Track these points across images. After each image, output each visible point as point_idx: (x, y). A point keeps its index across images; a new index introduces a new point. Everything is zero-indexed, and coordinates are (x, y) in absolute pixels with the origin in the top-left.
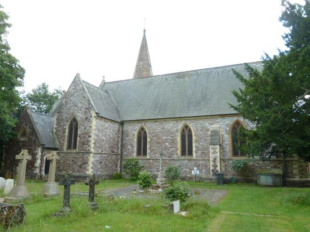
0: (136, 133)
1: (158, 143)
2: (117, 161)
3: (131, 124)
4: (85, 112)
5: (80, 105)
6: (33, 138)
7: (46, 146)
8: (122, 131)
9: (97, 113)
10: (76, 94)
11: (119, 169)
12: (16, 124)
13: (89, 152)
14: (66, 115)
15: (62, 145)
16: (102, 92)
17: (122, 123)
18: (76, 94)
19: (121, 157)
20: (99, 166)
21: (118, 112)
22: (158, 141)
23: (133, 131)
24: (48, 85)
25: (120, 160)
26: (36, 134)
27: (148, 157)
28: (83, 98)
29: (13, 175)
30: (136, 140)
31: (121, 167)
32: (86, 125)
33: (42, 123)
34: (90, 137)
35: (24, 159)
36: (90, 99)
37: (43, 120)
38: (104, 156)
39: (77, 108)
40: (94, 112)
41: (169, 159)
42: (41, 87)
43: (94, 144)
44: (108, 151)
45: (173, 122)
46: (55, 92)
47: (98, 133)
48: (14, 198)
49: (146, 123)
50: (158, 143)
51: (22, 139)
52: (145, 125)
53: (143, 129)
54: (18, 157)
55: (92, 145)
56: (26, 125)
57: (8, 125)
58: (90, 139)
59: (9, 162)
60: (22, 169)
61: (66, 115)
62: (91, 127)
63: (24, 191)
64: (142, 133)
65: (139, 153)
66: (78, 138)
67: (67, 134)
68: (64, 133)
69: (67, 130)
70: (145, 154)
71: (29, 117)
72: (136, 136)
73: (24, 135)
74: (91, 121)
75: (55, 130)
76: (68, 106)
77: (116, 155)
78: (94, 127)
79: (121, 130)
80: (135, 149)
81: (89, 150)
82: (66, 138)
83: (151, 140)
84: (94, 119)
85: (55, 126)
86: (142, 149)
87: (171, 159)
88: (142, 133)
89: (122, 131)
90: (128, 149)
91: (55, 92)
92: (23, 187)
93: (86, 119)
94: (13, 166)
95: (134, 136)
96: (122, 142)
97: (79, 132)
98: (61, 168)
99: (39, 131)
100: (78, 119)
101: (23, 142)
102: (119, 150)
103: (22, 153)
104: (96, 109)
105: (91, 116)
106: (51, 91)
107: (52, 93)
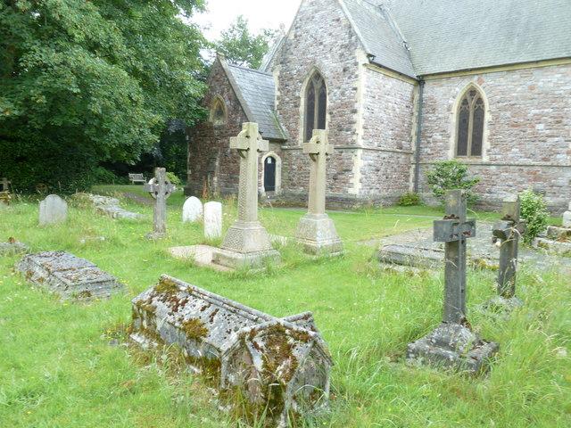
0: (455, 104)
1: (516, 125)
2: (409, 168)
3: (444, 82)
4: (342, 55)
5: (328, 40)
6: (239, 120)
7: (375, 61)
8: (421, 100)
9: (369, 56)
10: (317, 16)
11: (412, 185)
12: (205, 91)
13: (352, 147)
14: (298, 67)
15: (294, 133)
16: (373, 11)
17: (420, 81)
18: (317, 16)
19: (418, 158)
20: (374, 178)
21: (410, 56)
22: (516, 119)
23: (447, 98)
24: (247, 21)
25: (414, 166)
26: (243, 110)
27: (485, 158)
28: (334, 23)
29: (229, 190)
30: (454, 119)
31: (416, 181)
32: (344, 86)
33: (251, 88)
34: (355, 112)
35: (251, 149)
36: (352, 22)
37: (251, 81)
38: (384, 155)
39: (321, 47)
40: (363, 52)
41: (543, 163)
42: (236, 23)
43: (364, 128)
44: (390, 144)
45: (563, 70)
46: (262, 34)
47: (373, 102)
48: (240, 257)
49: (484, 77)
50: (516, 125)
51: (217, 123)
52: (480, 82)
53: (473, 92)
54: (236, 143)
55: (360, 132)
56: (222, 94)
57: (190, 95)
58: (355, 117)
59: (198, 167)
60: (251, 176)
61: (298, 67)
62: (355, 89)
63: (260, 234)
64: (472, 103)
65: (461, 150)
66: (328, 117)
67: (302, 109)
68: (296, 106)
69: (303, 101)
70: (477, 151)
71: (226, 76)
72: (455, 110)
73: (220, 113)
74: (356, 76)
75: (277, 103)
76: (301, 46)
77: (407, 154)
78: (362, 90)
79: (417, 96)
80: (453, 141)
81: (353, 142)
82: (302, 117)
83: (496, 118)
84: (364, 69)
85: (278, 93)
86: (470, 140)
87: (548, 163)
88: (472, 103)
89: (421, 100)
90: (435, 142)
91: (262, 34)
92: (255, 227)
93: (344, 70)
94: (207, 177)
95: (449, 110)
96: (419, 126)
97: (329, 104)
98: (295, 179)
99: (248, 103)
100: (326, 73)
101: (219, 128)
102: (413, 143)
103: (244, 131)
104: (366, 46)
105: (356, 64)
106: (253, 32)
107: (257, 35)
